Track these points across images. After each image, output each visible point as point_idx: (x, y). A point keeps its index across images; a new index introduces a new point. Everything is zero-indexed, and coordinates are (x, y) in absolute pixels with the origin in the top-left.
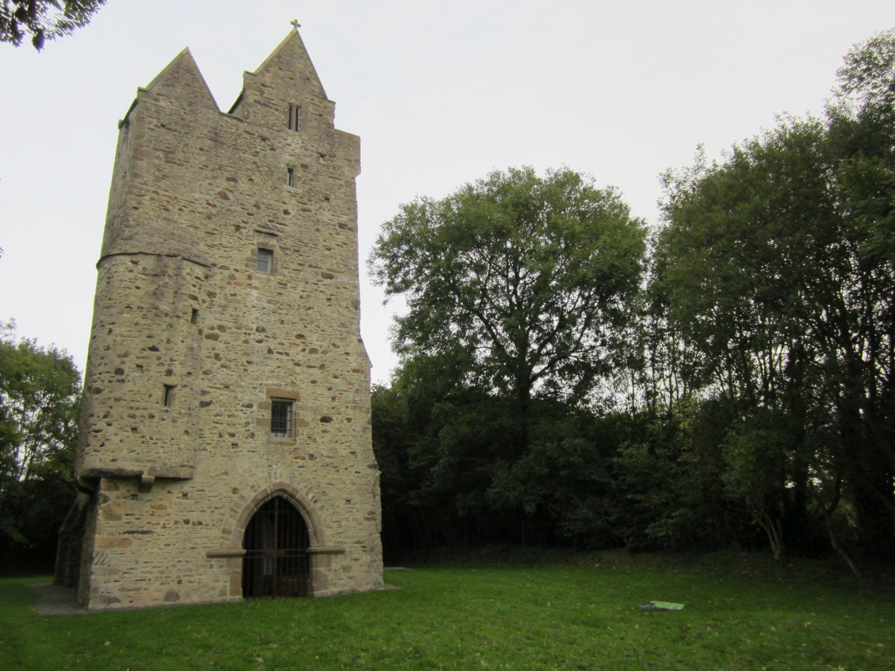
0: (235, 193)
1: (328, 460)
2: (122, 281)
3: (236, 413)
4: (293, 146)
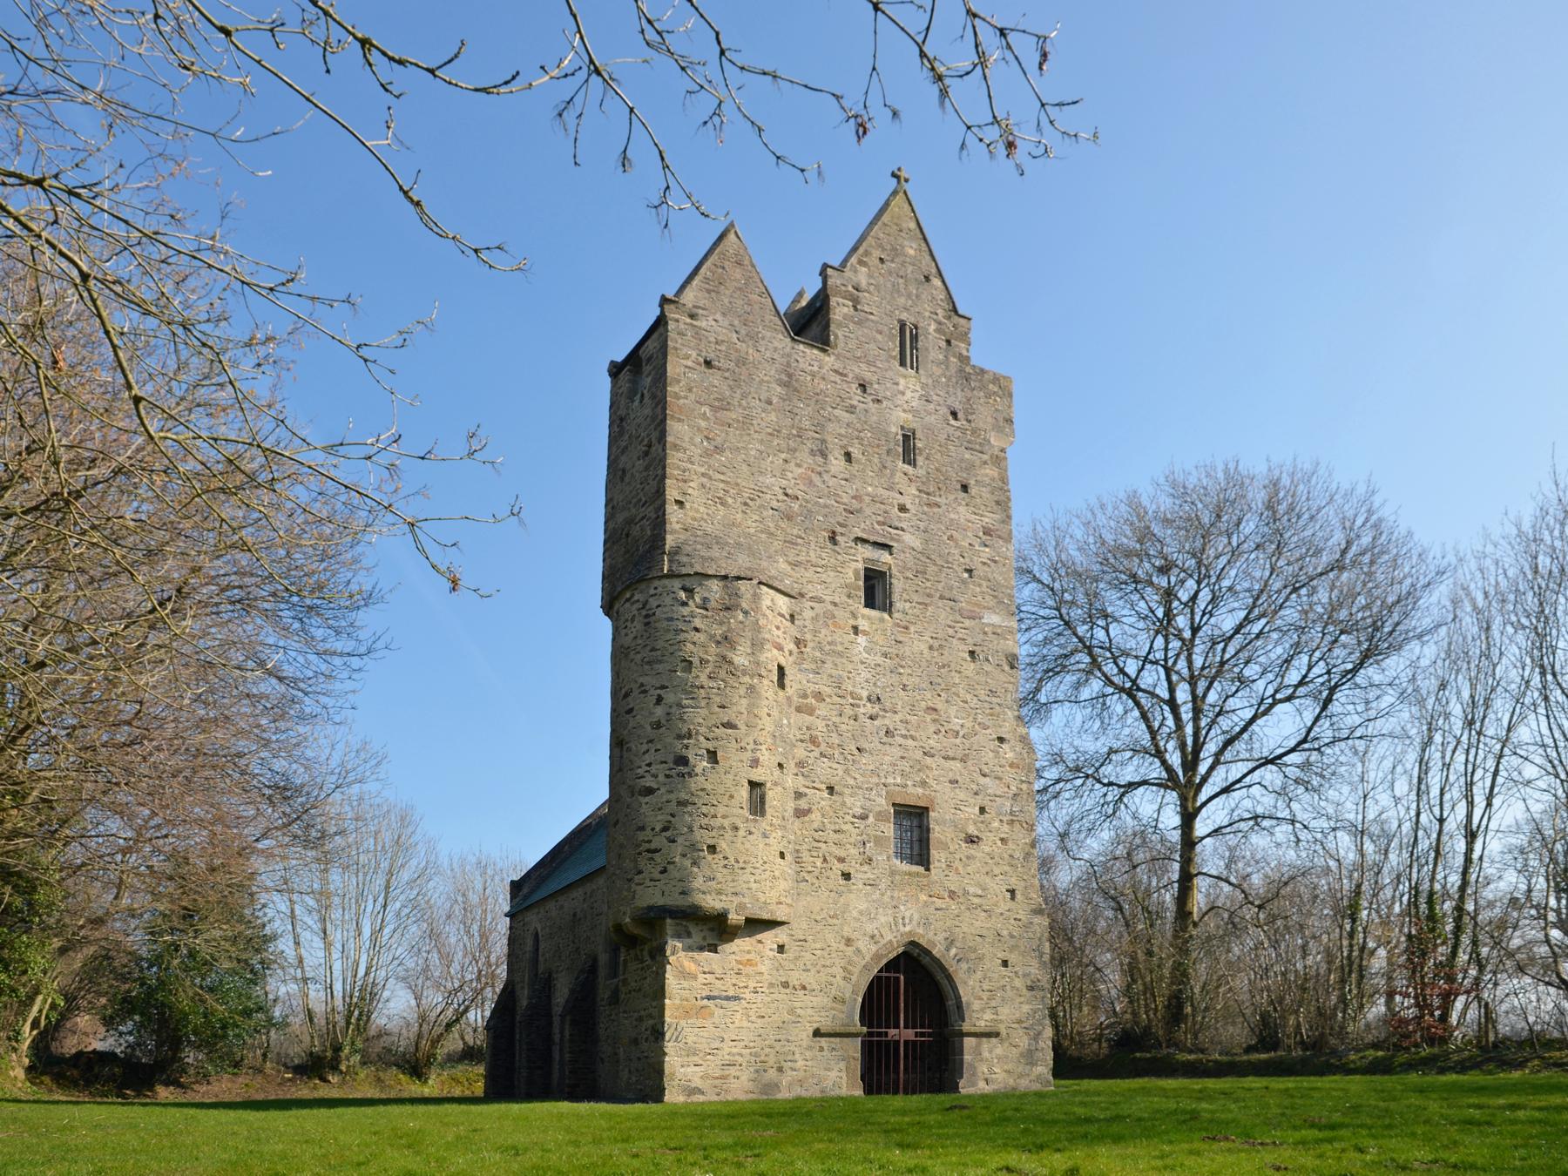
0: (826, 477)
1: (976, 900)
2: (671, 619)
3: (845, 827)
4: (909, 394)
